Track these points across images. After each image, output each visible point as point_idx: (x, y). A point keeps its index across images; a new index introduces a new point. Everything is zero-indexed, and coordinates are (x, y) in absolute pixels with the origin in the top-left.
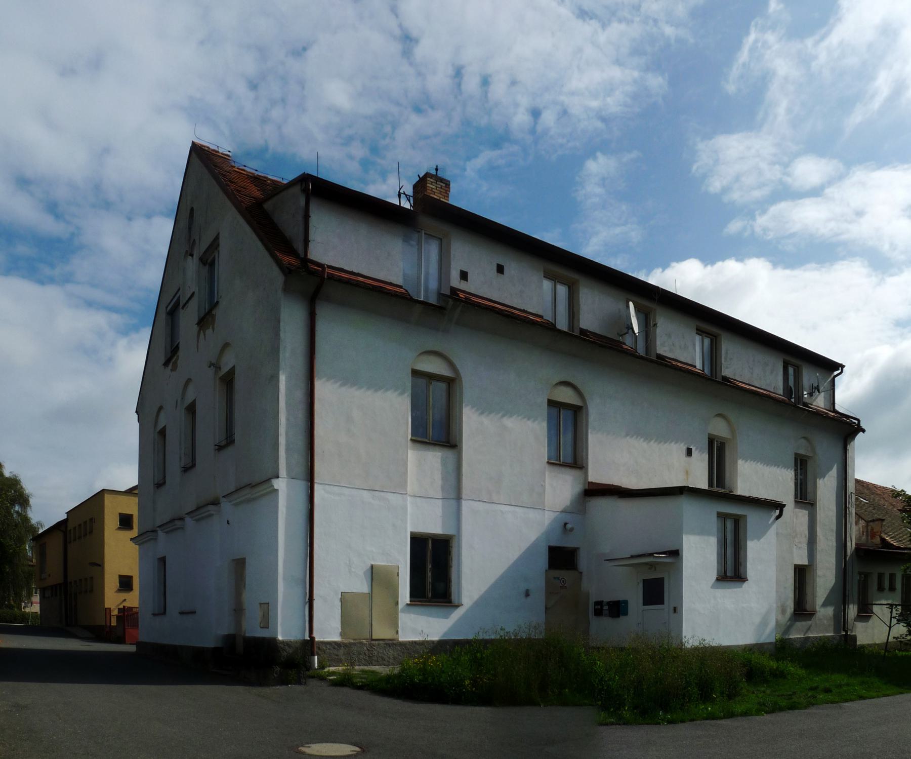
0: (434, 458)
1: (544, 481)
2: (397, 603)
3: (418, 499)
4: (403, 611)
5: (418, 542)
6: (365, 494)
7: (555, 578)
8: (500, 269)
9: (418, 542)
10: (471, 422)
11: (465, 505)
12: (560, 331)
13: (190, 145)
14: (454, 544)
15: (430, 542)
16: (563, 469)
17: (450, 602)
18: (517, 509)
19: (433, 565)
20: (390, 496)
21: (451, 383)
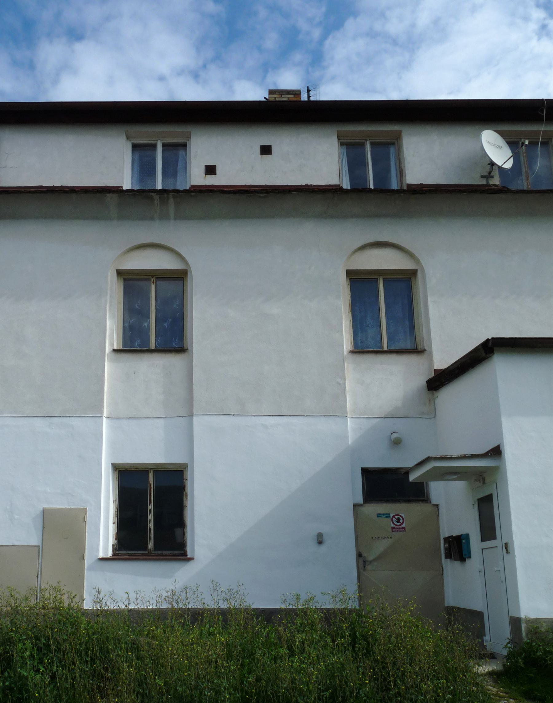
0: (153, 369)
1: (343, 378)
2: (83, 558)
3: (125, 422)
4: (91, 568)
5: (130, 479)
6: (39, 423)
7: (379, 516)
8: (266, 150)
9: (130, 479)
10: (203, 316)
11: (199, 423)
12: (347, 191)
13: (496, 445)
14: (188, 475)
15: (151, 476)
16: (366, 356)
17: (185, 554)
18: (294, 420)
19: (153, 511)
20: (76, 422)
21: (177, 278)
